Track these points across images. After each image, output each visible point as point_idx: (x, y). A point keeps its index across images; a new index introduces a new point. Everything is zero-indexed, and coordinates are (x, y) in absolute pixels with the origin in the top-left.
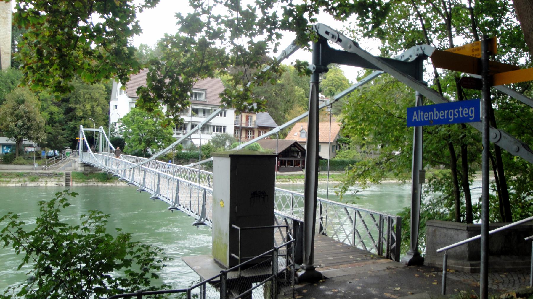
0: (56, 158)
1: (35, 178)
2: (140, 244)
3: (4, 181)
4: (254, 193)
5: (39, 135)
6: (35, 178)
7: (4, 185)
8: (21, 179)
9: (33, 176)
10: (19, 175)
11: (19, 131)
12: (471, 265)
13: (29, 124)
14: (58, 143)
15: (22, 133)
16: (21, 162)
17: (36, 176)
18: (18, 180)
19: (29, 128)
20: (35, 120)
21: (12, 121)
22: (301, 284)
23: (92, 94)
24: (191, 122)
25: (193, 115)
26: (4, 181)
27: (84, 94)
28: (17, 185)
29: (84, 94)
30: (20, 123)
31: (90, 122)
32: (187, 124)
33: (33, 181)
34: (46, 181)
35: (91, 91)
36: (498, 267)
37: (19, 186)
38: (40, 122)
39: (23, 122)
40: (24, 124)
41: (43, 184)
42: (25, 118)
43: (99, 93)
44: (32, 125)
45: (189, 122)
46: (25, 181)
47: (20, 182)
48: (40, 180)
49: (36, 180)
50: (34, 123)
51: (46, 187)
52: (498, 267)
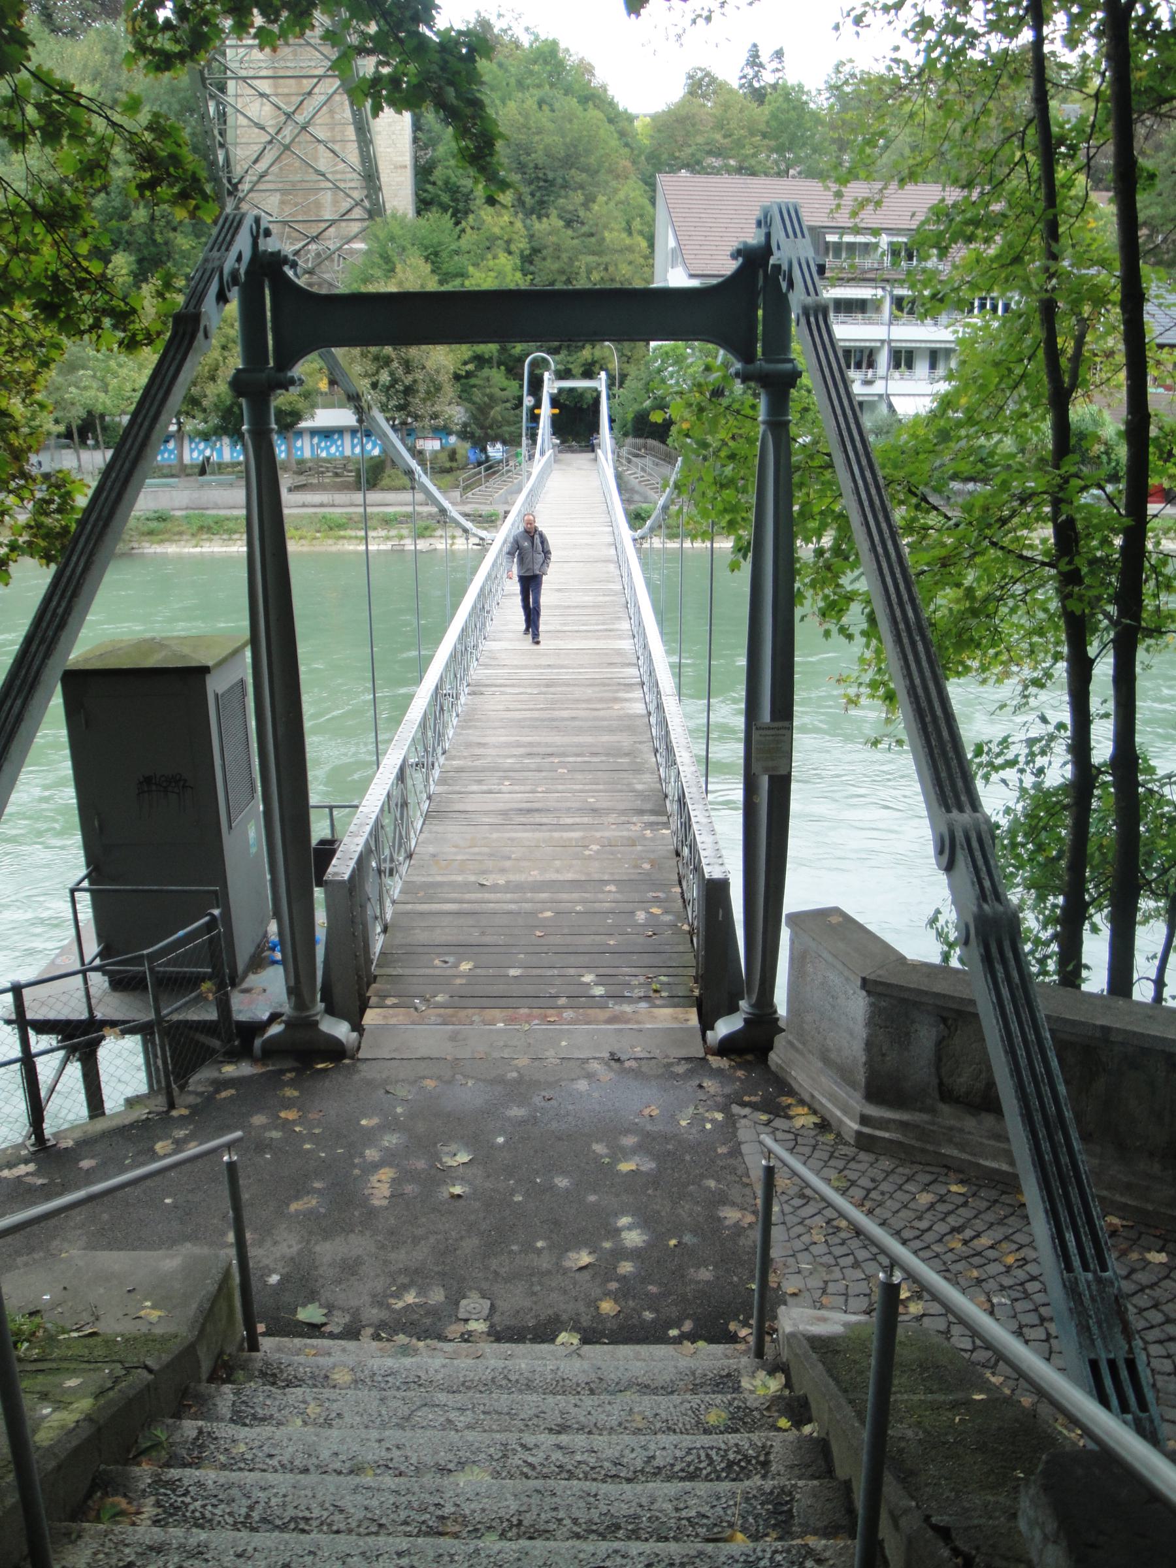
0: (487, 469)
1: (426, 528)
2: (992, 681)
3: (351, 538)
4: (148, 780)
5: (437, 408)
6: (426, 528)
7: (351, 548)
8: (393, 533)
9: (421, 524)
10: (387, 522)
11: (384, 399)
12: (864, 1120)
13: (408, 380)
14: (491, 427)
15: (392, 403)
16: (397, 483)
17: (427, 523)
18: (383, 533)
19: (409, 391)
20: (424, 368)
21: (366, 375)
22: (264, 1065)
23: (611, 269)
24: (890, 341)
25: (896, 318)
26: (351, 538)
27: (589, 272)
28: (383, 547)
29: (589, 272)
30: (384, 377)
31: (607, 353)
32: (879, 349)
33: (419, 535)
34: (453, 537)
35: (606, 259)
36: (955, 1153)
37: (386, 551)
38: (438, 371)
39: (392, 374)
40: (395, 381)
41: (440, 545)
42: (395, 364)
43: (630, 263)
44: (415, 381)
45: (883, 341)
46: (401, 537)
47: (388, 538)
48: (439, 533)
49: (427, 533)
50: (419, 375)
51: (453, 552)
52: (955, 1153)
